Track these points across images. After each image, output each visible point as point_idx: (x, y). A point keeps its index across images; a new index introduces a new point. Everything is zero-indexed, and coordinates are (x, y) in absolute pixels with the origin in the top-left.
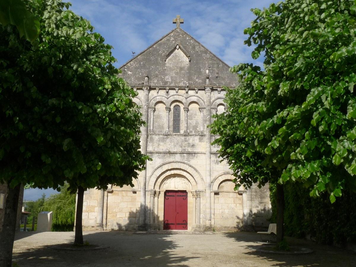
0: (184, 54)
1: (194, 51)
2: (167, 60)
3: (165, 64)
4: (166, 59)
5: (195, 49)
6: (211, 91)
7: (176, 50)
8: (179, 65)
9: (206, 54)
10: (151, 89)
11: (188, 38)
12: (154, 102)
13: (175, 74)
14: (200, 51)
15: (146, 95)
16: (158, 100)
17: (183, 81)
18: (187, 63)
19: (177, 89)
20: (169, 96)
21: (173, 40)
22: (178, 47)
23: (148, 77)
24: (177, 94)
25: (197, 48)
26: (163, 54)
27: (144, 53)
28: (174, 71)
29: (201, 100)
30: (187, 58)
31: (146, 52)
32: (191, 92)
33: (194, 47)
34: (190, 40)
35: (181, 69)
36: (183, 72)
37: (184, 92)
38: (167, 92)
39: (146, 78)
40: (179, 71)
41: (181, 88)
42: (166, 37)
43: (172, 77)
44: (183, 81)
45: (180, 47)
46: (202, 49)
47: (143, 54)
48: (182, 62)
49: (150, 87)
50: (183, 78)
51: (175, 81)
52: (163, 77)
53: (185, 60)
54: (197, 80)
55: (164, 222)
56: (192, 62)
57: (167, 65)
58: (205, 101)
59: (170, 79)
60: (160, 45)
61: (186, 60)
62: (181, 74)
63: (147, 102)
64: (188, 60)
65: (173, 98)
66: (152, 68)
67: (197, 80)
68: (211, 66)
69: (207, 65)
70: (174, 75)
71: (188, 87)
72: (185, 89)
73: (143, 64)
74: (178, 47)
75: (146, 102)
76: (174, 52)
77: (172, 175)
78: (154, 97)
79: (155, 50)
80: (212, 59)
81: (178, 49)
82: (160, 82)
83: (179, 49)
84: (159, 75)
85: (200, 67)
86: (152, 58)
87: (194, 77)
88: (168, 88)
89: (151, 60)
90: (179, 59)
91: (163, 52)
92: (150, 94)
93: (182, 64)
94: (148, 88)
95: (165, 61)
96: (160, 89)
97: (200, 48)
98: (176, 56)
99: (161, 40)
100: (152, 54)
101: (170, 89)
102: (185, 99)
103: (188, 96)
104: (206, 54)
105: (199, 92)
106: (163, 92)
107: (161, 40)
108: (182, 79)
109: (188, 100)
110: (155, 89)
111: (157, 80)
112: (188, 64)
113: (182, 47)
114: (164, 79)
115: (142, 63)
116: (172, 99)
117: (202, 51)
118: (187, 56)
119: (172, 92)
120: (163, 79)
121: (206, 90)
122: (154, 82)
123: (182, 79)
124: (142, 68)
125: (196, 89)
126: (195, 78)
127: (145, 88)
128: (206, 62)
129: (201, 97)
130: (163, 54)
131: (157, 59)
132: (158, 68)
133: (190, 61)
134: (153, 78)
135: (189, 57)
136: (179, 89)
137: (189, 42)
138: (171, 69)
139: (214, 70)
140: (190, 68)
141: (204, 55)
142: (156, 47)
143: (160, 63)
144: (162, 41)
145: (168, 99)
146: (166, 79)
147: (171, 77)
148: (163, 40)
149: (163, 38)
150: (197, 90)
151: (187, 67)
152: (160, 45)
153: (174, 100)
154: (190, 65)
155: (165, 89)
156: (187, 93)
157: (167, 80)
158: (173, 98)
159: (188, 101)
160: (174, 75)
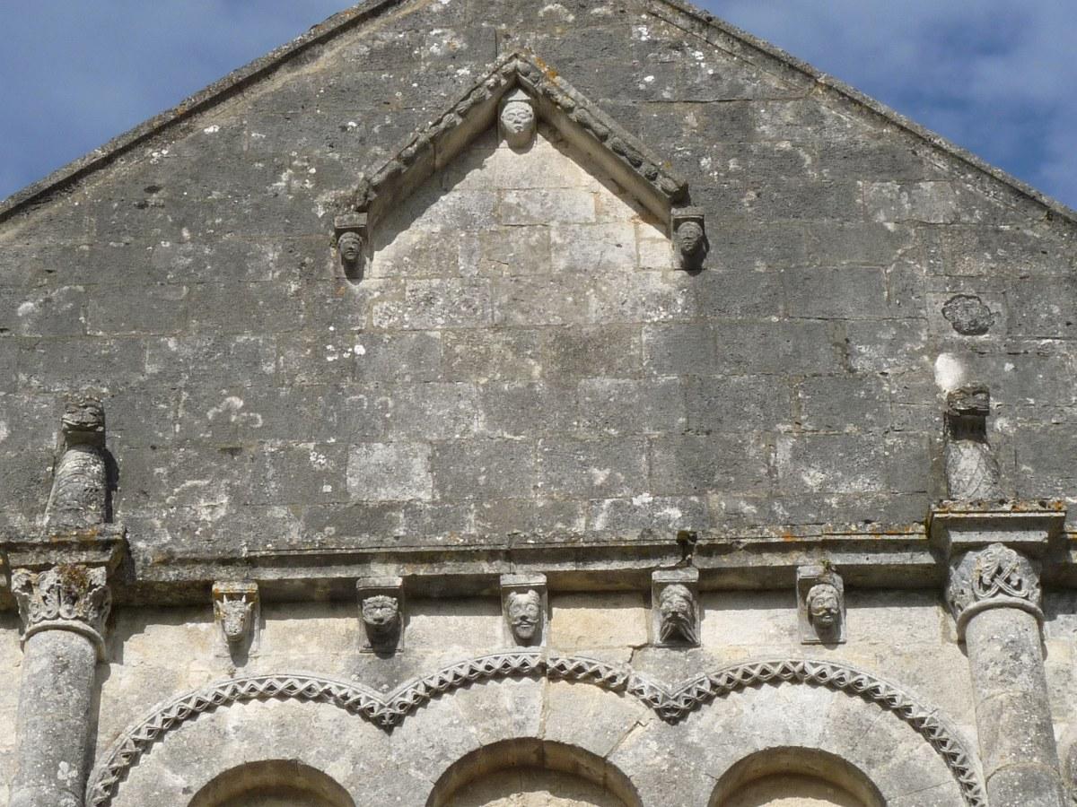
0: (606, 193)
1: (742, 153)
2: (379, 263)
3: (349, 306)
4: (369, 238)
5: (748, 131)
6: (1031, 592)
7: (504, 151)
8: (551, 311)
9: (908, 183)
10: (133, 599)
11: (644, 33)
12: (179, 781)
13: (496, 419)
14: (826, 155)
15: (61, 666)
16: (235, 754)
17: (604, 491)
18: (656, 284)
19: (525, 578)
20: (407, 690)
21: (454, 56)
22: (517, 110)
23: (87, 437)
24: (533, 656)
25: (775, 126)
26: (328, 196)
27: (74, 200)
28: (473, 386)
29: (900, 730)
30: (650, 231)
31: (88, 189)
32: (735, 635)
33: (732, 119)
34: (677, 46)
35: (578, 352)
36: (603, 383)
37: (629, 625)
38: (383, 639)
39: (73, 460)
40: (554, 381)
41: (595, 576)
42: (365, 31)
43: (444, 458)
44: (604, 491)
45: (543, 122)
46: (847, 128)
47: (55, 207)
48: (580, 277)
49: (121, 557)
50: (609, 454)
51: (490, 493)
52: (318, 460)
53: (619, 258)
54: (813, 478)
55: (372, 247)
56: (715, 265)
57: (379, 316)
58: (967, 732)
59: (419, 467)
60: (289, 107)
61: (644, 254)
62: (574, 411)
63: (67, 772)
64: (660, 251)
65: (477, 717)
66: (171, 359)
67: (813, 478)
68: (996, 307)
69: (935, 303)
70: (478, 426)
71: (684, 545)
72: (640, 591)
73: (47, 317)
74: (517, 110)
75: (50, 769)
76: (474, 175)
77: (868, 551)
78: (174, 702)
79: (221, 159)
80: (987, 238)
81: (522, 145)
82: (279, 512)
83: (542, 146)
84: (269, 431)
85: (834, 319)
86: (175, 250)
87: (772, 438)
88: (389, 575)
89: (154, 276)
90: (547, 247)
91: (316, 177)
92: (120, 680)
93: (581, 304)
94: (98, 576)
95: (354, 269)
96: (272, 602)
97: (815, 118)
98: (499, 213)
99: (295, 56)
100: (174, 204)
101: (417, 596)
102: (649, 715)
103: (702, 679)
104: (908, 183)
105: (860, 621)
106: (314, 647)
107: (295, 56)
108: (600, 476)
109: (694, 737)
110: (192, 602)
111: (234, 493)
112: (665, 301)
113: (568, 93)
114: (337, 477)
115: (26, 307)
116: (453, 729)
117: (851, 155)
118: (648, 215)
119: (445, 642)
120: (320, 477)
121: (963, 577)
122: (184, 516)
123: (600, 476)
124: (22, 366)
125: (808, 567)
126: (783, 454)
127: (51, 577)
128: (922, 271)
129: (902, 693)
130: (328, 196)
131: (236, 261)
132: (253, 359)
133: (693, 260)
134: (174, 477)
135: (681, 197)
136: (555, 593)
137: (664, 70)
138: (434, 365)
139: (1042, 355)
140: (696, 343)
141: (869, 189)
142: (231, 135)
143: (279, 301)
144: (310, 69)
145: (388, 724)
146: (368, 482)
147: (442, 447)
148: (327, 58)
149: (324, 40)
150: (826, 595)
151: (665, 327)
152: (289, 107)
153: (478, 736)
154: (699, 301)
155: (343, 598)
156: (679, 635)
157: (384, 494)
158: (477, 717)
159: (696, 752)
160: (478, 426)
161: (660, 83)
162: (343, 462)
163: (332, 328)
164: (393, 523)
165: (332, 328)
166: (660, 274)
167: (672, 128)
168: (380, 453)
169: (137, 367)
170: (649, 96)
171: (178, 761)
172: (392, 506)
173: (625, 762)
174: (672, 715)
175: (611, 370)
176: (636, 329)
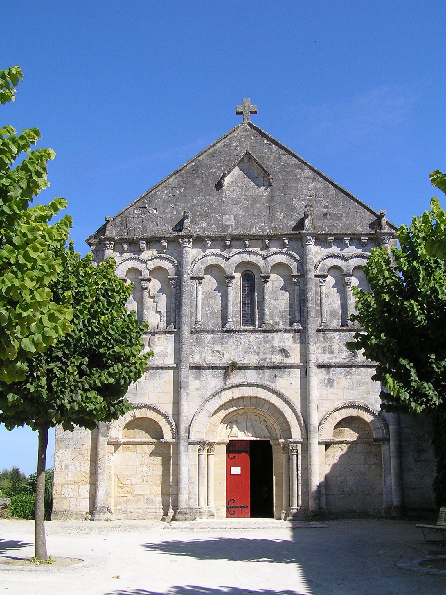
13: (243, 211)
16: (209, 263)
36: (258, 205)
43: (236, 217)
57: (227, 193)
70: (241, 212)
84: (212, 213)
114: (222, 221)
138: (236, 202)
147: (236, 216)
148: (218, 145)
157: (228, 223)
160: (241, 212)
161: (268, 151)
162: (222, 218)
163: (386, 314)
164: (229, 228)
165: (386, 314)
166: (29, 469)
167: (269, 159)
168: (227, 217)
169: (193, 202)
170: (266, 154)
171: (202, 263)
172: (229, 225)
173: (259, 264)
174: (265, 258)
175: (260, 203)
176: (262, 196)
